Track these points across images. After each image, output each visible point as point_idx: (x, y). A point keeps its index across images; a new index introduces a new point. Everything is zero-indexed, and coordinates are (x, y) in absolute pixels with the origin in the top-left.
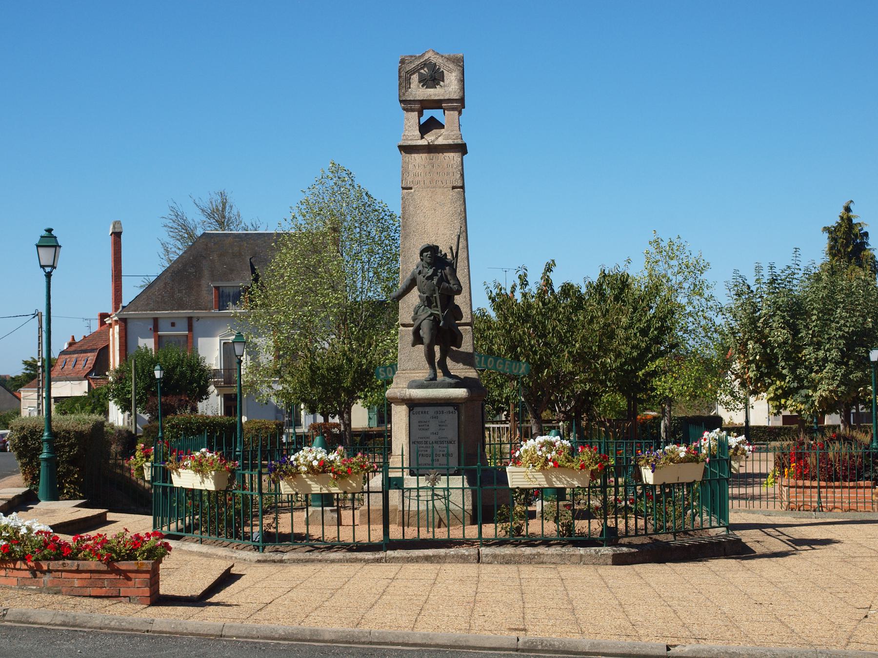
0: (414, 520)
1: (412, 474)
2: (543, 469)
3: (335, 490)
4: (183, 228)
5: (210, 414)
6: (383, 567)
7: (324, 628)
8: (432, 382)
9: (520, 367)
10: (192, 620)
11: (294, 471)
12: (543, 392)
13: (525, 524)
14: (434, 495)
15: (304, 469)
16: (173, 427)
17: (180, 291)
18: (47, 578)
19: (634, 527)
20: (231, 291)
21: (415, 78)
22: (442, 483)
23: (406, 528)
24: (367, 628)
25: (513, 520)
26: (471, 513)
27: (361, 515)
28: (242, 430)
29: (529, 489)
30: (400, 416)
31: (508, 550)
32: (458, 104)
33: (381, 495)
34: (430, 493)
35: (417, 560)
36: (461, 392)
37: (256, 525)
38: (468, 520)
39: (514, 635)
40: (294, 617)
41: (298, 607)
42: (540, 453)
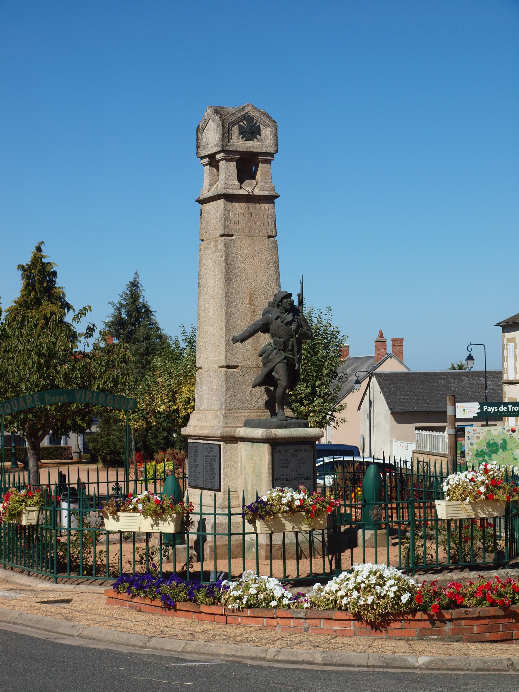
18: (448, 627)
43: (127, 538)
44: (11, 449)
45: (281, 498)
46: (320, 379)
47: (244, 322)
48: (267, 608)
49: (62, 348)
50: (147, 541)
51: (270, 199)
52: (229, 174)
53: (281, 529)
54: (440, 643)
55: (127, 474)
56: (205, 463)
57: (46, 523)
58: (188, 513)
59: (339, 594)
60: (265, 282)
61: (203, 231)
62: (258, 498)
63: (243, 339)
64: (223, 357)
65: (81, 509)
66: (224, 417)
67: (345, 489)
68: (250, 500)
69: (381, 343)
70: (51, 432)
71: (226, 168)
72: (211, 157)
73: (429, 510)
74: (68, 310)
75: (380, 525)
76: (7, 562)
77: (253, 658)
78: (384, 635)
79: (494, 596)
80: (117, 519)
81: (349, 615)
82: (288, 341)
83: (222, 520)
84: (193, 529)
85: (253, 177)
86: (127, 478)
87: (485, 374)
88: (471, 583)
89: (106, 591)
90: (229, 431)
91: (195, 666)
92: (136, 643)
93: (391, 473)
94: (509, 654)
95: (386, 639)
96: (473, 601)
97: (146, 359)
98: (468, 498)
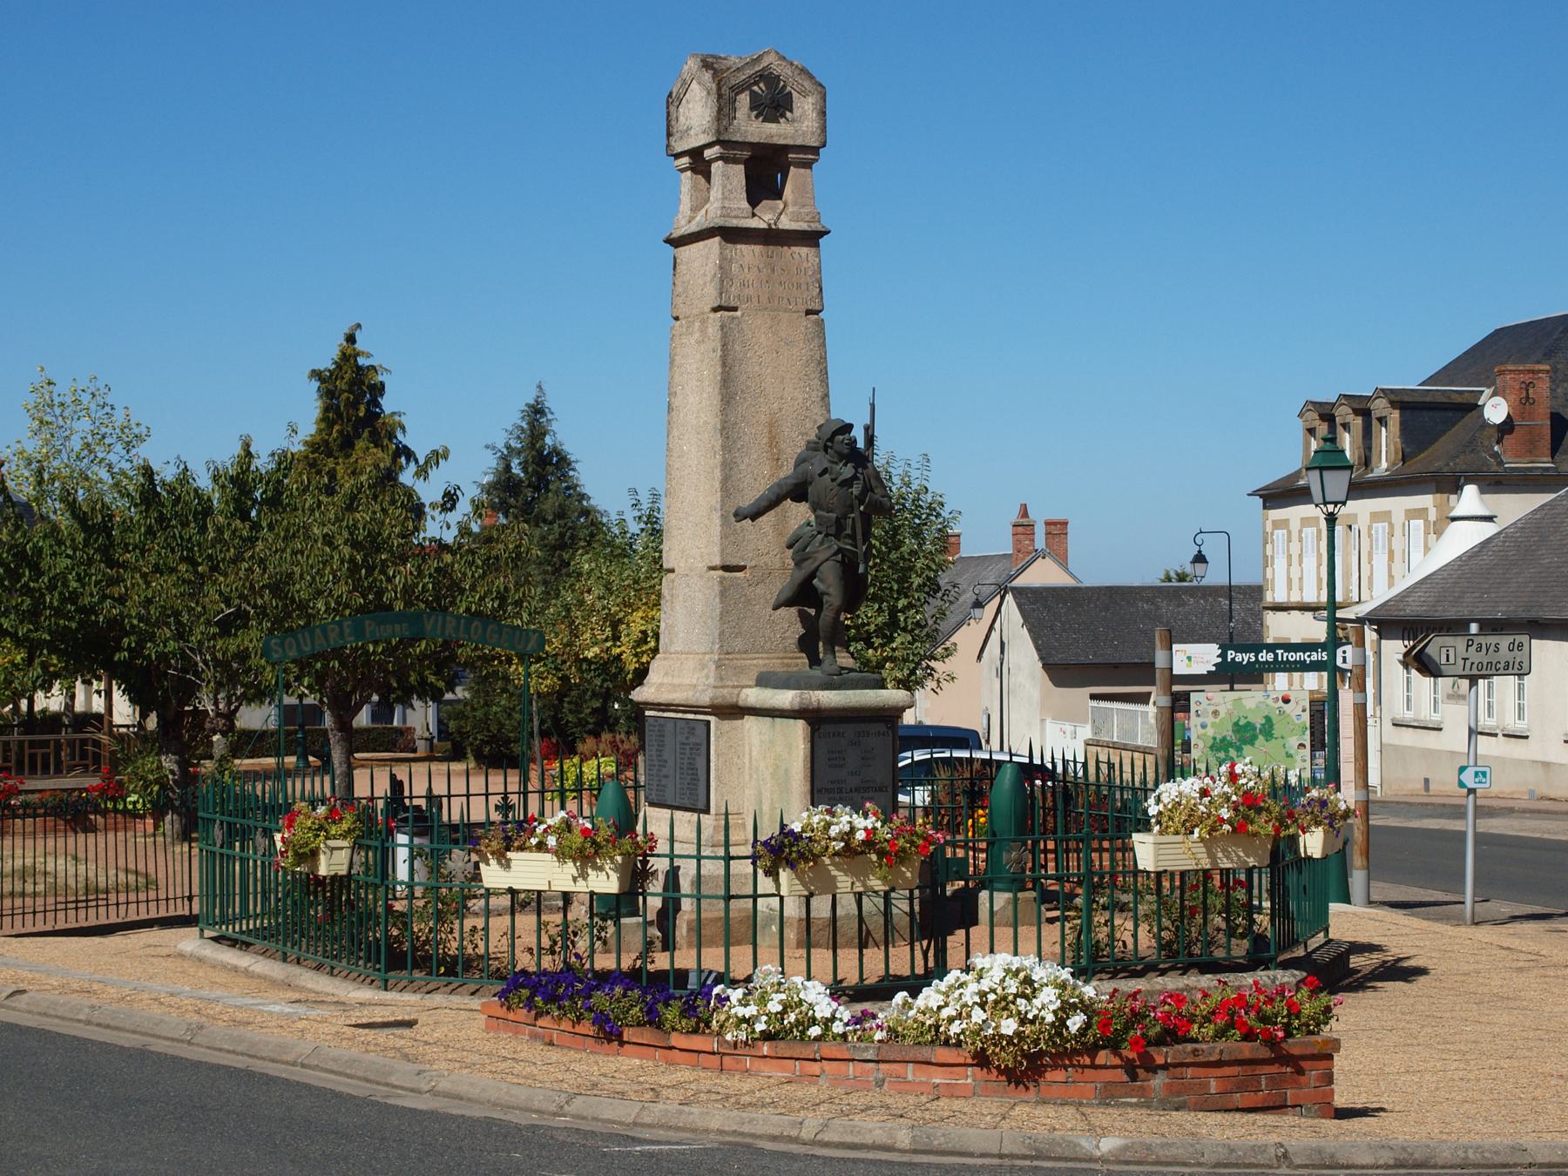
18: (1159, 1081)
43: (524, 905)
44: (296, 732)
45: (828, 825)
46: (906, 597)
47: (757, 481)
48: (802, 1039)
49: (397, 530)
50: (565, 910)
51: (811, 238)
53: (830, 887)
54: (1144, 1111)
55: (525, 780)
56: (677, 760)
57: (366, 873)
58: (645, 855)
59: (945, 1013)
61: (679, 300)
62: (783, 826)
63: (755, 514)
64: (716, 549)
65: (435, 845)
66: (718, 667)
67: (955, 811)
68: (768, 831)
69: (1023, 527)
70: (375, 698)
71: (726, 176)
72: (696, 154)
73: (1119, 855)
74: (408, 461)
75: (1023, 881)
76: (288, 949)
77: (774, 1138)
78: (1032, 1095)
79: (1251, 1019)
80: (507, 865)
81: (964, 1055)
82: (845, 517)
83: (713, 868)
84: (656, 886)
85: (778, 194)
86: (525, 787)
87: (1230, 591)
88: (1205, 995)
89: (483, 1005)
90: (727, 695)
91: (661, 1152)
92: (544, 1106)
93: (1044, 782)
94: (1279, 1135)
95: (1037, 1103)
96: (1209, 1030)
97: (560, 556)
98: (1197, 830)
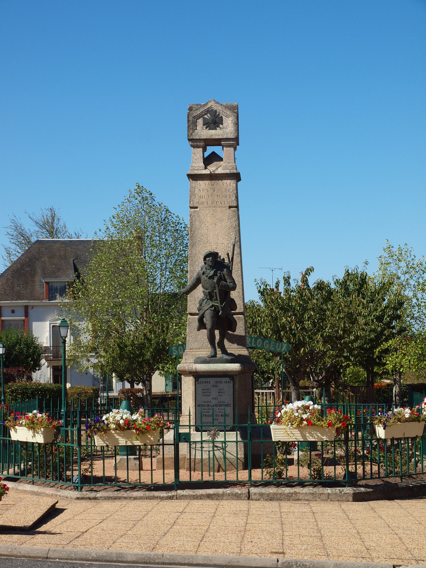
0: (198, 466)
1: (197, 430)
2: (298, 426)
3: (137, 443)
4: (21, 235)
5: (42, 382)
6: (175, 503)
7: (127, 551)
8: (213, 359)
9: (282, 347)
10: (24, 545)
11: (105, 428)
12: (301, 365)
13: (285, 470)
14: (214, 446)
15: (113, 426)
16: (12, 392)
17: (18, 286)
19: (370, 472)
20: (58, 286)
21: (200, 122)
22: (220, 438)
23: (192, 472)
24: (160, 552)
25: (276, 466)
26: (243, 460)
27: (158, 462)
28: (66, 394)
29: (289, 442)
30: (188, 385)
31: (272, 490)
32: (234, 142)
33: (173, 446)
34: (211, 445)
35: (201, 497)
36: (236, 367)
37: (76, 470)
38: (241, 466)
39: (275, 557)
40: (104, 543)
41: (108, 535)
42: (296, 414)
52: (195, 158)
60: (226, 244)
